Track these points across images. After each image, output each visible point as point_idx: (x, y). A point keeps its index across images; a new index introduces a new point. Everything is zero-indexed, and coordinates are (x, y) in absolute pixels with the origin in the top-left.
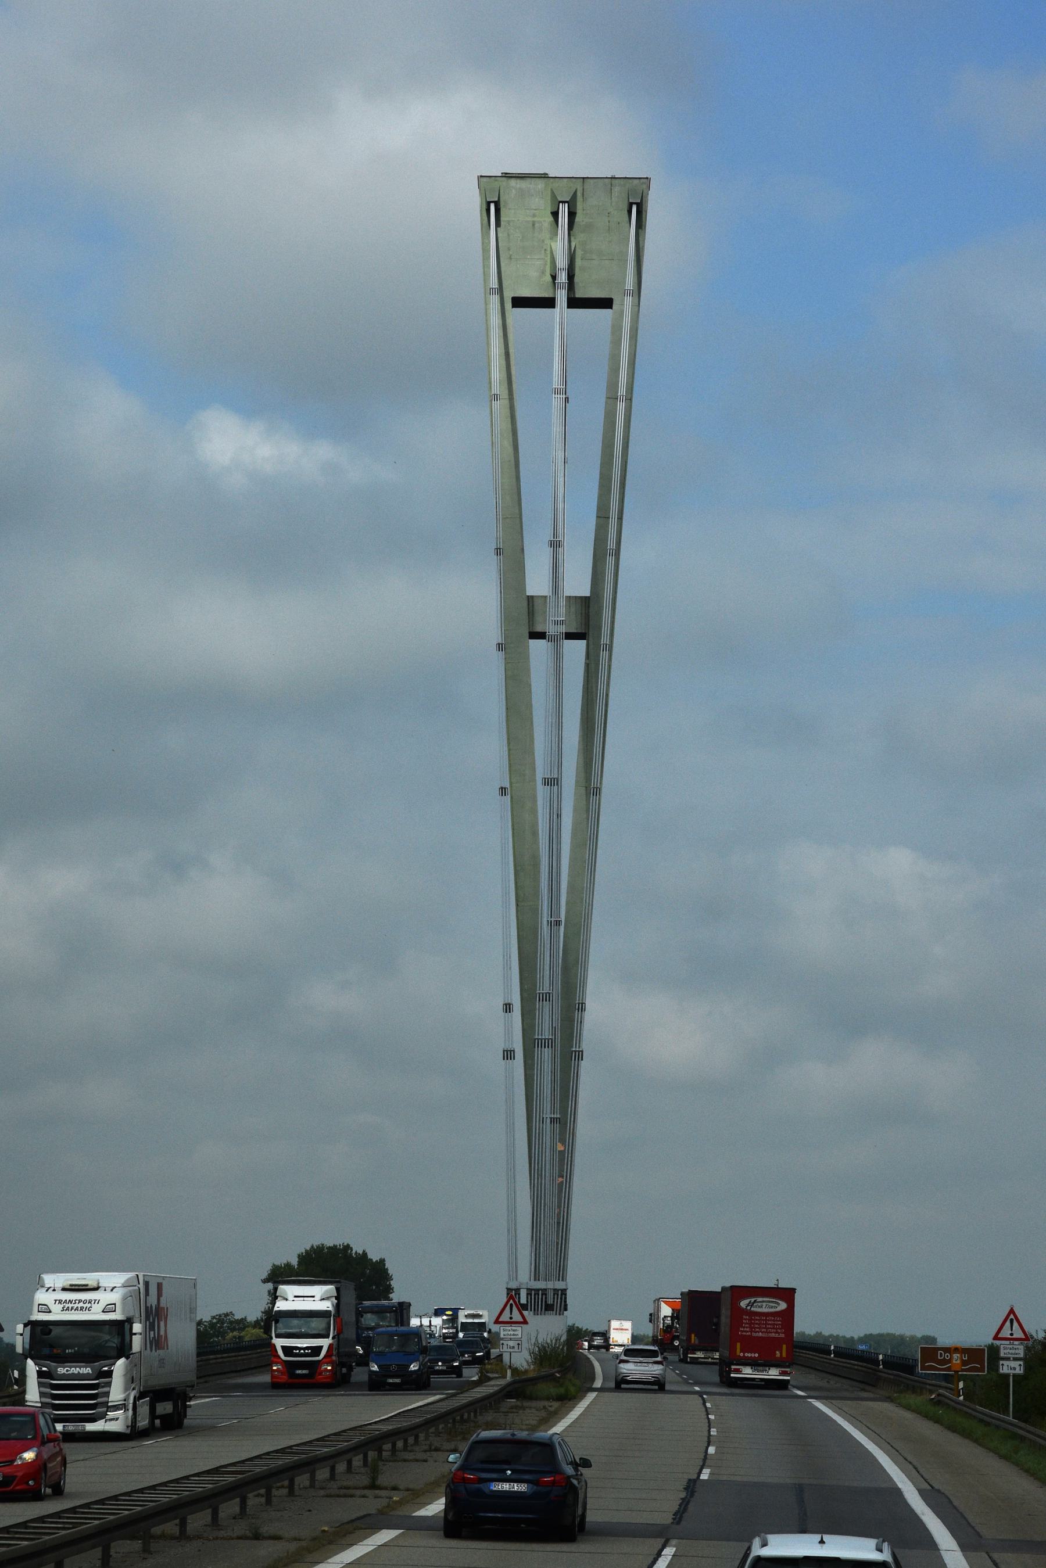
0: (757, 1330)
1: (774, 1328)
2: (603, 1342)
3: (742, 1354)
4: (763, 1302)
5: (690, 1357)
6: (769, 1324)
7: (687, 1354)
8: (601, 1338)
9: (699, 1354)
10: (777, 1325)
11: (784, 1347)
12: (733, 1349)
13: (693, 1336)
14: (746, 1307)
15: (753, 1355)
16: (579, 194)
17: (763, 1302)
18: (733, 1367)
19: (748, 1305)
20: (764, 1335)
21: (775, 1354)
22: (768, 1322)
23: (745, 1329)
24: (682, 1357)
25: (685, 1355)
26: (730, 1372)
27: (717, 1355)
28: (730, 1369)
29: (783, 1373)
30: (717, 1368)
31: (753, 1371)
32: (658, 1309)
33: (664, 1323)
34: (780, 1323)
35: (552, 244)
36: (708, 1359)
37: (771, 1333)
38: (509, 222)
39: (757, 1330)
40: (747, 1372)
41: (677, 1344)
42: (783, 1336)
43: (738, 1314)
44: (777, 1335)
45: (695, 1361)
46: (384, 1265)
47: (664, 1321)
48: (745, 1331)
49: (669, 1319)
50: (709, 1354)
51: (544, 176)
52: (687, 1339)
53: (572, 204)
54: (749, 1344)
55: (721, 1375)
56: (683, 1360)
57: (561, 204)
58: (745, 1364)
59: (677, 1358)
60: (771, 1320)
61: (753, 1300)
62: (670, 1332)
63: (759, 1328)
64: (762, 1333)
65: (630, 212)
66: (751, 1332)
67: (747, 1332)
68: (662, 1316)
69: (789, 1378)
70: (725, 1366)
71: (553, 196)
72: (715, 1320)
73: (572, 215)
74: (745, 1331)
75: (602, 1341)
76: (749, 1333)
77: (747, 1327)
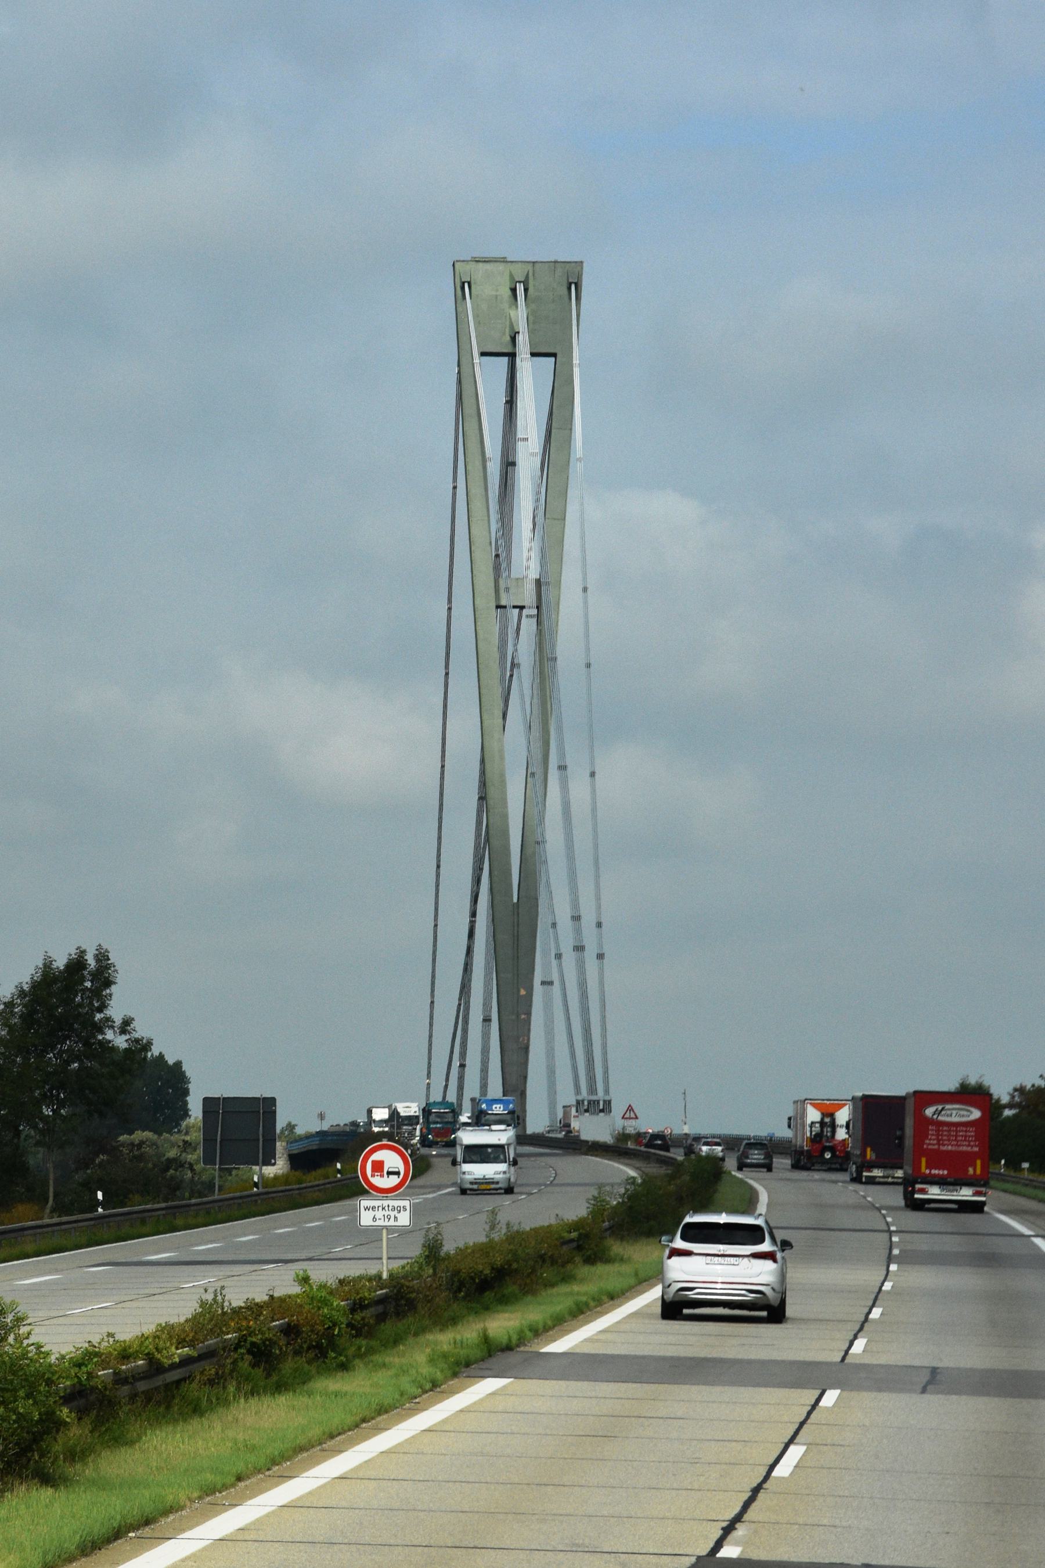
0: (946, 1142)
1: (965, 1140)
2: (764, 1159)
3: (928, 1171)
4: (953, 1109)
5: (866, 1177)
6: (960, 1136)
7: (862, 1172)
8: (760, 1152)
9: (877, 1173)
10: (969, 1136)
11: (979, 1162)
12: (917, 1166)
13: (869, 1150)
14: (933, 1115)
15: (941, 1172)
16: (531, 274)
17: (953, 1109)
18: (918, 1186)
19: (934, 1114)
20: (954, 1148)
21: (968, 1171)
22: (964, 1133)
23: (932, 1142)
24: (855, 1175)
25: (859, 1173)
26: (913, 1192)
27: (899, 1173)
28: (913, 1188)
29: (977, 1193)
30: (901, 1189)
31: (941, 1191)
32: (803, 1114)
33: (811, 1132)
34: (972, 1134)
35: (511, 312)
36: (888, 1177)
37: (963, 1145)
38: (477, 296)
39: (946, 1142)
40: (934, 1192)
41: (829, 1156)
42: (976, 1149)
43: (923, 1124)
44: (969, 1149)
45: (872, 1181)
46: (181, 1067)
47: (811, 1127)
48: (931, 1143)
49: (818, 1125)
50: (890, 1172)
51: (504, 261)
52: (861, 1154)
53: (526, 283)
54: (937, 1159)
55: (905, 1198)
56: (857, 1179)
57: (518, 284)
58: (932, 1183)
59: (848, 1179)
60: (962, 1131)
61: (940, 1107)
62: (820, 1142)
63: (949, 1140)
64: (952, 1146)
65: (569, 289)
66: (939, 1144)
67: (934, 1145)
68: (809, 1122)
69: (983, 1199)
70: (909, 1185)
71: (511, 276)
72: (898, 1133)
73: (526, 290)
74: (931, 1143)
75: (762, 1157)
76: (936, 1147)
77: (934, 1140)
